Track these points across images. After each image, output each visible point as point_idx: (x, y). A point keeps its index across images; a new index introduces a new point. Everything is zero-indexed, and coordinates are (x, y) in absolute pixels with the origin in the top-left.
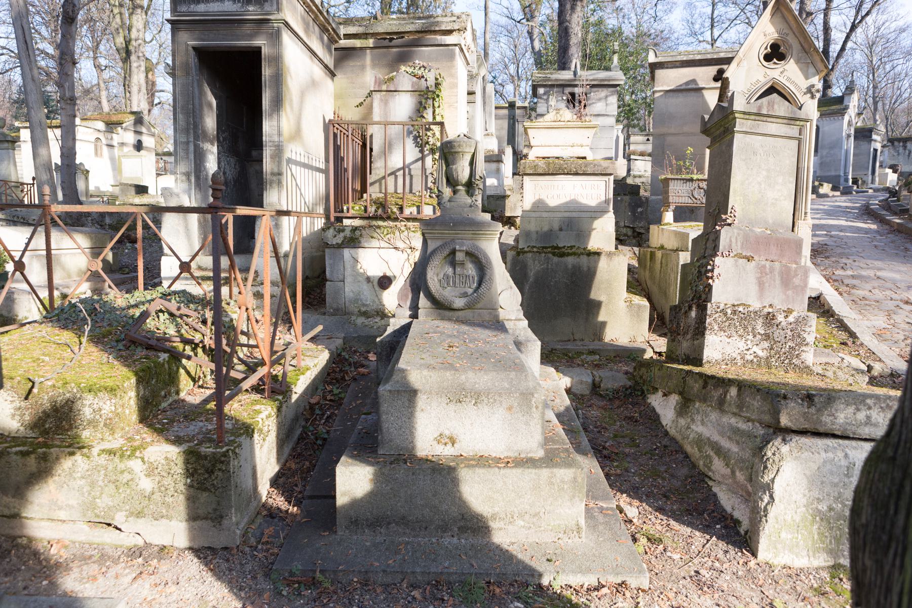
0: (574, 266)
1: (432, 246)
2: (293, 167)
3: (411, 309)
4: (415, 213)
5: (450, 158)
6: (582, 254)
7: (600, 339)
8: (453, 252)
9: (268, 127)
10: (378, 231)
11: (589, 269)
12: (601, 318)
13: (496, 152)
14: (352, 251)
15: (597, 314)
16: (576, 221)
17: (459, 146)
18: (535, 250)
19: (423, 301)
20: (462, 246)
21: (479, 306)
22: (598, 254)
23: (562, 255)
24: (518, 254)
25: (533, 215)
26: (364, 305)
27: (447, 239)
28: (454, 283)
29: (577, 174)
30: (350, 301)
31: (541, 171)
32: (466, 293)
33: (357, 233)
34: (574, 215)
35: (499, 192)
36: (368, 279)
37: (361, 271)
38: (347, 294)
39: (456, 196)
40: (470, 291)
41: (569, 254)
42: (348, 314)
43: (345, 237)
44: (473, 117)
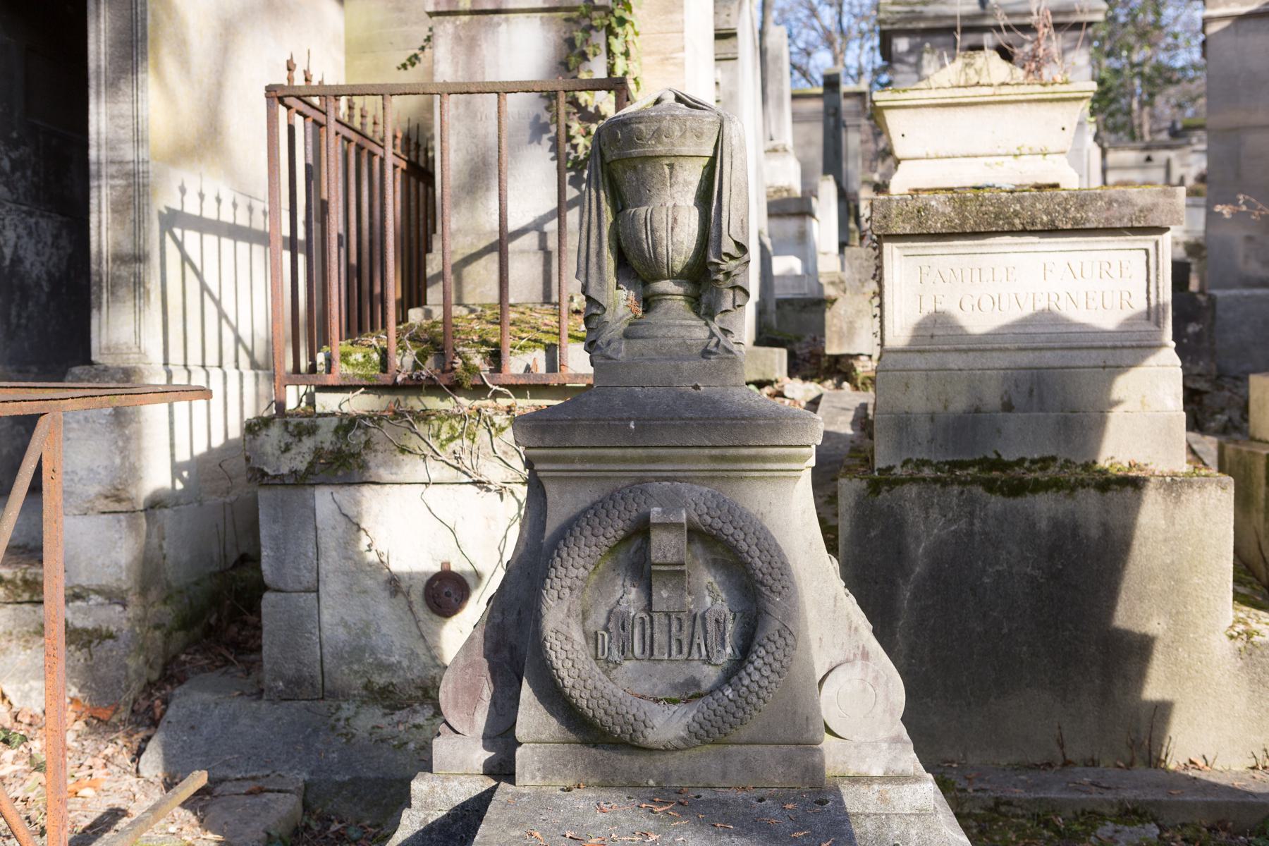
0: (1056, 525)
2: (191, 239)
3: (489, 739)
4: (541, 368)
5: (627, 179)
6: (1083, 484)
7: (1153, 760)
8: (641, 530)
9: (102, 118)
10: (422, 428)
11: (1106, 529)
12: (1153, 691)
13: (797, 190)
14: (343, 494)
15: (1140, 677)
16: (1056, 377)
17: (657, 134)
18: (927, 472)
19: (532, 716)
21: (744, 733)
22: (1133, 484)
23: (1017, 489)
24: (875, 487)
25: (919, 361)
26: (382, 667)
27: (626, 466)
29: (1052, 231)
31: (938, 227)
32: (694, 682)
34: (1050, 359)
35: (806, 291)
36: (394, 584)
37: (372, 557)
38: (327, 632)
39: (655, 317)
40: (709, 675)
41: (1038, 487)
42: (333, 694)
43: (318, 453)
44: (732, 96)
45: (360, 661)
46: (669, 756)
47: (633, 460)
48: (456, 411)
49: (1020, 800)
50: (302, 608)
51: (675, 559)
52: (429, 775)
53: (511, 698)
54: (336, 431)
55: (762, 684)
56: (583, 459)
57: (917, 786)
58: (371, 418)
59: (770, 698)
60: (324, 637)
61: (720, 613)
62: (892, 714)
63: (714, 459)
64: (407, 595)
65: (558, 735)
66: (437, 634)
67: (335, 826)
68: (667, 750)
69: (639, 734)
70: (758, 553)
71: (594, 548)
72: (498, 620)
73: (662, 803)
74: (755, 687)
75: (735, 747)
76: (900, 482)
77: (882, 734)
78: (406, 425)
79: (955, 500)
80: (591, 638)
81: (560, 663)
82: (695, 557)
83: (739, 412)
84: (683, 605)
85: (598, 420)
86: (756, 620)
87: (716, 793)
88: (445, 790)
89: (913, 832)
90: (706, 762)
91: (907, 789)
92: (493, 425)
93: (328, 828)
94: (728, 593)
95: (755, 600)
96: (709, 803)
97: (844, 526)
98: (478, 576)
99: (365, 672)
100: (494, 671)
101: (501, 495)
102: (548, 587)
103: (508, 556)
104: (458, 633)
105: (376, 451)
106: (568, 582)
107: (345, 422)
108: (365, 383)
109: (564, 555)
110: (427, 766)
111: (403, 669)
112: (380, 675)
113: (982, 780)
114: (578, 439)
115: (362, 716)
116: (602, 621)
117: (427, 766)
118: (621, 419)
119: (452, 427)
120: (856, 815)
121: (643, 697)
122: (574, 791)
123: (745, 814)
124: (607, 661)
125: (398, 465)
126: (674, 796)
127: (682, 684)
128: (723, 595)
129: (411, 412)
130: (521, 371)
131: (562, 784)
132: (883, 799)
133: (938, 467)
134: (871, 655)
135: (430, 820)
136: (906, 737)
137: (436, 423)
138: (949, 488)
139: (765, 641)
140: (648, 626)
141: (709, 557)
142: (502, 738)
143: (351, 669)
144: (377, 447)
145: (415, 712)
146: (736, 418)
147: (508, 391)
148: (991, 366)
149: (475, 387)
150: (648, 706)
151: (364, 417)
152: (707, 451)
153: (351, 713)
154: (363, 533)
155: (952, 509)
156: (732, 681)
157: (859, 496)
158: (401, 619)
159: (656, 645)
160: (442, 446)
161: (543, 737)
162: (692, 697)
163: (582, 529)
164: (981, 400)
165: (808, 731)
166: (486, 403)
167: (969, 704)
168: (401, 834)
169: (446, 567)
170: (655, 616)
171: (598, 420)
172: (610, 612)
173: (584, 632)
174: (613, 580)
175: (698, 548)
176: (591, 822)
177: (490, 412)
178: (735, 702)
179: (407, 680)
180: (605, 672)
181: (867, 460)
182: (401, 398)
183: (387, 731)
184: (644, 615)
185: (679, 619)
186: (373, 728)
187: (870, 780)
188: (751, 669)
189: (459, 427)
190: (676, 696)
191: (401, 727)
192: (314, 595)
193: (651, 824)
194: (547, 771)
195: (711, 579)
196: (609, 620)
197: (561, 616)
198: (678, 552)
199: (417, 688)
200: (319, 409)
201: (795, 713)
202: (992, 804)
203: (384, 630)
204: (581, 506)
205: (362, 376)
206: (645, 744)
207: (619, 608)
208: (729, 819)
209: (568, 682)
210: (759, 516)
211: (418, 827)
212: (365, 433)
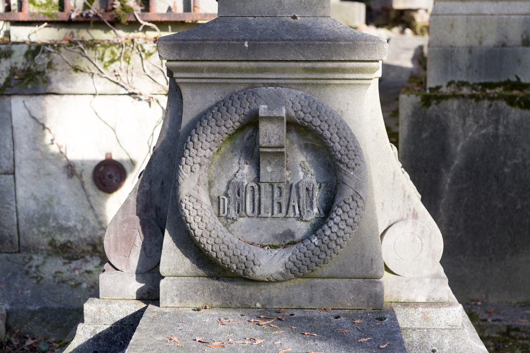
1: (194, 104)
3: (141, 274)
8: (252, 122)
14: (32, 102)
18: (465, 91)
20: (275, 107)
21: (326, 270)
24: (427, 101)
26: (62, 229)
28: (258, 207)
30: (30, 221)
32: (290, 233)
33: (41, 60)
36: (71, 169)
37: (54, 149)
38: (21, 204)
40: (301, 228)
43: (13, 71)
45: (46, 225)
46: (271, 286)
47: (247, 71)
48: (116, 41)
49: (525, 327)
50: (3, 186)
51: (277, 144)
52: (97, 299)
53: (156, 245)
54: (26, 55)
55: (339, 235)
56: (210, 70)
57: (450, 309)
58: (52, 45)
59: (345, 244)
60: (19, 207)
61: (309, 184)
62: (433, 258)
63: (307, 70)
64: (80, 176)
65: (190, 270)
66: (102, 205)
67: (29, 342)
68: (270, 281)
69: (250, 270)
70: (338, 139)
71: (217, 135)
72: (147, 189)
73: (266, 319)
74: (334, 237)
75: (319, 280)
76: (445, 97)
77: (426, 272)
78: (79, 50)
79: (485, 111)
80: (216, 201)
81: (192, 218)
82: (292, 143)
83: (326, 35)
84: (283, 177)
85: (221, 40)
86: (336, 189)
87: (305, 312)
88: (109, 310)
89: (446, 341)
90: (298, 291)
91: (443, 311)
92: (143, 51)
93: (24, 343)
94: (315, 170)
95: (336, 175)
96: (300, 319)
97: (403, 130)
98: (133, 163)
99: (50, 233)
100: (144, 225)
101: (150, 103)
102: (184, 163)
103: (154, 144)
104: (118, 203)
105: (56, 70)
106: (198, 160)
107: (33, 48)
108: (47, 19)
109: (196, 140)
110: (94, 292)
111: (78, 231)
112: (61, 235)
113: (498, 313)
114: (206, 55)
115: (48, 265)
116: (223, 189)
117: (94, 292)
118: (238, 40)
119: (113, 53)
120: (406, 329)
121: (252, 244)
122: (203, 310)
123: (325, 327)
124: (227, 218)
125: (73, 80)
126: (275, 314)
127: (281, 235)
128: (312, 171)
129: (82, 41)
130: (165, 11)
131: (193, 305)
132: (426, 318)
133: (473, 87)
134: (419, 215)
135: (98, 331)
136: (444, 275)
137: (101, 49)
138: (481, 102)
139: (342, 203)
140: (256, 193)
141: (302, 142)
142: (150, 274)
143: (39, 231)
144: (57, 67)
145: (87, 261)
146: (323, 40)
147: (154, 26)
148: (515, 11)
149: (130, 23)
150: (256, 250)
151: (47, 45)
152: (301, 65)
153: (40, 262)
154: (47, 131)
155: (483, 117)
156: (318, 232)
157: (415, 108)
158: (76, 194)
159: (262, 206)
160: (105, 66)
161: (180, 272)
162: (288, 244)
163: (208, 121)
164: (506, 37)
165: (372, 269)
166: (138, 35)
167: (491, 260)
168: (76, 342)
169: (109, 156)
170: (262, 186)
171: (221, 40)
172: (229, 182)
173: (210, 197)
174: (231, 159)
175: (294, 136)
176: (214, 331)
177: (141, 41)
178: (319, 247)
179: (80, 239)
180: (225, 226)
181: (421, 83)
182: (74, 30)
183: (66, 275)
184: (254, 184)
185: (280, 188)
186: (56, 273)
187: (416, 305)
188: (331, 223)
189: (118, 52)
190: (277, 243)
191: (77, 272)
192: (11, 176)
193: (258, 332)
194: (183, 297)
195: (303, 159)
196: (228, 188)
197: (193, 184)
198: (279, 138)
199: (89, 244)
200: (13, 39)
201: (363, 256)
202: (504, 330)
203: (64, 202)
204: (208, 105)
205: (45, 14)
206: (253, 277)
207: (235, 180)
208: (313, 330)
209: (198, 232)
210: (339, 113)
211: (89, 336)
212: (48, 57)
